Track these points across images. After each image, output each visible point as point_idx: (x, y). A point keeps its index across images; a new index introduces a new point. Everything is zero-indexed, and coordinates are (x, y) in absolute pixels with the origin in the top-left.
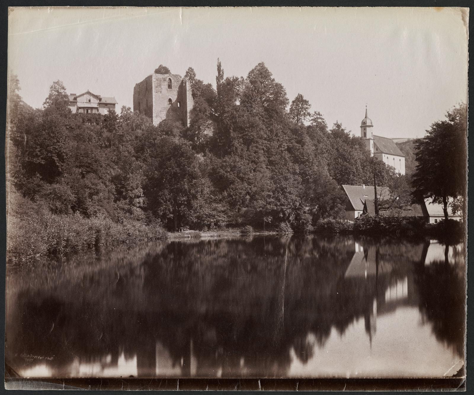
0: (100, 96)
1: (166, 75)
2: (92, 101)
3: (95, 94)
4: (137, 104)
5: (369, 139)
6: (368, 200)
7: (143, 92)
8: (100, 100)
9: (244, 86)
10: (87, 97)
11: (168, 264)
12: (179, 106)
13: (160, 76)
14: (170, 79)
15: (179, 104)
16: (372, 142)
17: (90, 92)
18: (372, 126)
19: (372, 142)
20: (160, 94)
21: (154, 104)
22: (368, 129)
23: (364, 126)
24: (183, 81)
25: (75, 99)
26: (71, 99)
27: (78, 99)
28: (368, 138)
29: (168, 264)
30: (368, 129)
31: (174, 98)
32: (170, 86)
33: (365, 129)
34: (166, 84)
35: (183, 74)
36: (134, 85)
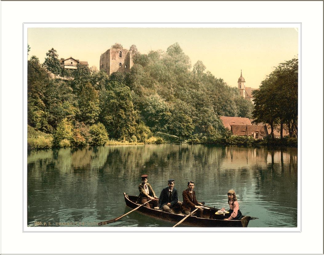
0: (79, 60)
1: (119, 49)
2: (73, 63)
3: (75, 59)
4: (102, 67)
5: (243, 89)
6: (233, 125)
7: (105, 58)
8: (78, 62)
9: (205, 194)
10: (70, 61)
11: (292, 165)
12: (126, 67)
13: (115, 50)
14: (121, 52)
15: (126, 66)
16: (244, 91)
17: (73, 58)
18: (245, 82)
19: (244, 91)
20: (115, 61)
21: (111, 66)
22: (242, 83)
23: (240, 81)
24: (128, 53)
25: (63, 62)
26: (61, 62)
27: (65, 62)
28: (242, 88)
29: (292, 165)
30: (242, 83)
31: (123, 63)
32: (121, 56)
33: (240, 83)
34: (119, 54)
35: (129, 49)
36: (101, 55)
